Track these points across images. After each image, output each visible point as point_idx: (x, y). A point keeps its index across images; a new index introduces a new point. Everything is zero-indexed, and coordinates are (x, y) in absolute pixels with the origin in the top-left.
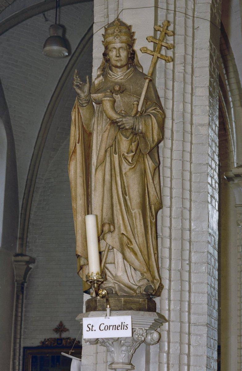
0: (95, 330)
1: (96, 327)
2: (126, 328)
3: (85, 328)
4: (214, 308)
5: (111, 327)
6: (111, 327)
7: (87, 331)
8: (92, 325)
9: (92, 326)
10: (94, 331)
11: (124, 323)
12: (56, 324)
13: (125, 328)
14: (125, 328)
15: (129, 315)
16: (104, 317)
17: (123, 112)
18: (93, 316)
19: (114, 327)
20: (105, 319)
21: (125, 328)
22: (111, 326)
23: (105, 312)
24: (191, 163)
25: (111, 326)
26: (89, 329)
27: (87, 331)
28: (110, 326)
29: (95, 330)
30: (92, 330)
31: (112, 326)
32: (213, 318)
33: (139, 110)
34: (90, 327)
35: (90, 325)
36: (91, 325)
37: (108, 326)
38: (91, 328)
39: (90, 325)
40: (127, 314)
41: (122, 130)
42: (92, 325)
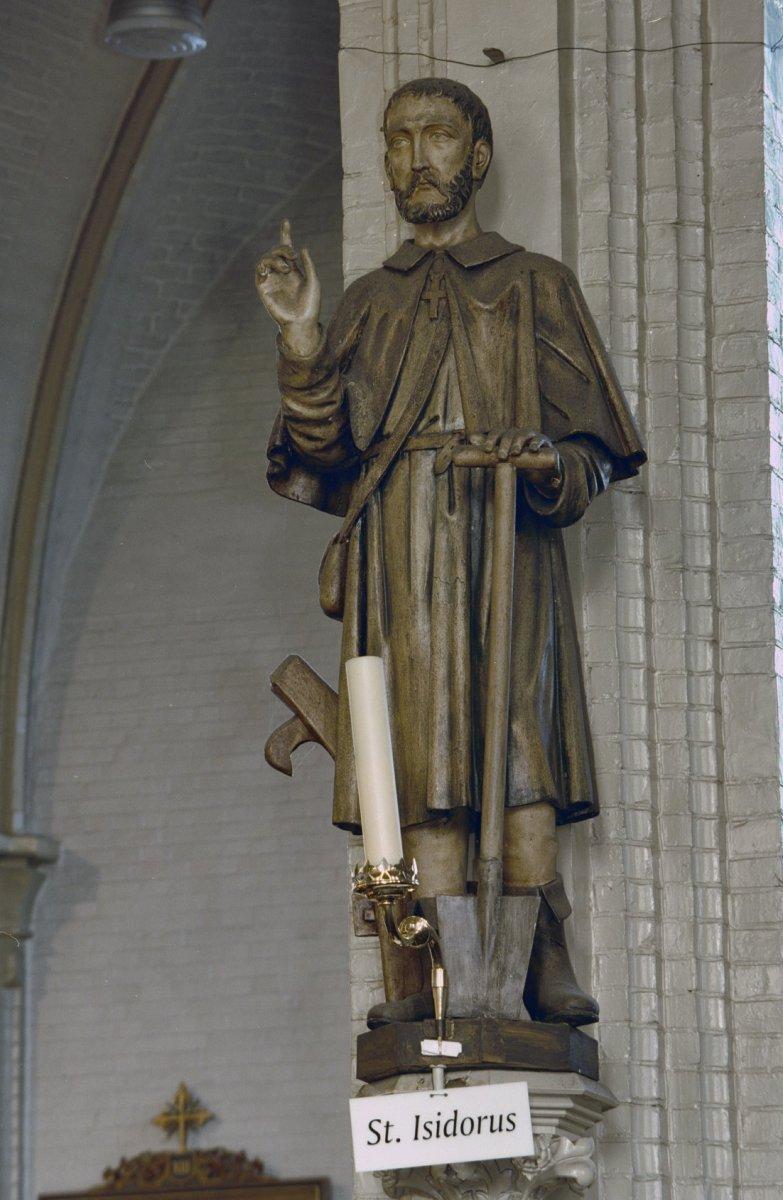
0: (398, 1140)
1: (403, 1128)
2: (510, 1127)
3: (360, 1135)
4: (778, 909)
5: (486, 1124)
6: (486, 1124)
7: (369, 1143)
8: (388, 1123)
9: (388, 1126)
10: (394, 1142)
11: (439, 1114)
12: (438, 1110)
13: (506, 1124)
14: (504, 1127)
15: (347, 1113)
16: (427, 1094)
17: (481, 156)
18: (407, 1089)
19: (496, 1126)
20: (431, 1100)
21: (506, 1124)
22: (486, 1117)
23: (427, 1077)
24: (711, 470)
25: (486, 1117)
26: (376, 1138)
27: (369, 1143)
28: (480, 1119)
29: (398, 1140)
30: (387, 1141)
31: (489, 1119)
32: (754, 262)
33: (570, 288)
34: (381, 1130)
35: (379, 1121)
36: (385, 1124)
37: (472, 1120)
38: (381, 1130)
39: (379, 1121)
40: (522, 1080)
41: (763, 1182)
42: (388, 1123)
